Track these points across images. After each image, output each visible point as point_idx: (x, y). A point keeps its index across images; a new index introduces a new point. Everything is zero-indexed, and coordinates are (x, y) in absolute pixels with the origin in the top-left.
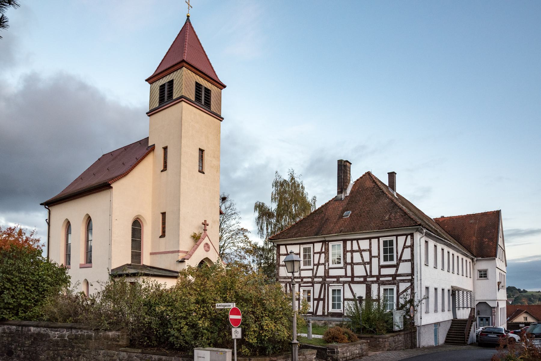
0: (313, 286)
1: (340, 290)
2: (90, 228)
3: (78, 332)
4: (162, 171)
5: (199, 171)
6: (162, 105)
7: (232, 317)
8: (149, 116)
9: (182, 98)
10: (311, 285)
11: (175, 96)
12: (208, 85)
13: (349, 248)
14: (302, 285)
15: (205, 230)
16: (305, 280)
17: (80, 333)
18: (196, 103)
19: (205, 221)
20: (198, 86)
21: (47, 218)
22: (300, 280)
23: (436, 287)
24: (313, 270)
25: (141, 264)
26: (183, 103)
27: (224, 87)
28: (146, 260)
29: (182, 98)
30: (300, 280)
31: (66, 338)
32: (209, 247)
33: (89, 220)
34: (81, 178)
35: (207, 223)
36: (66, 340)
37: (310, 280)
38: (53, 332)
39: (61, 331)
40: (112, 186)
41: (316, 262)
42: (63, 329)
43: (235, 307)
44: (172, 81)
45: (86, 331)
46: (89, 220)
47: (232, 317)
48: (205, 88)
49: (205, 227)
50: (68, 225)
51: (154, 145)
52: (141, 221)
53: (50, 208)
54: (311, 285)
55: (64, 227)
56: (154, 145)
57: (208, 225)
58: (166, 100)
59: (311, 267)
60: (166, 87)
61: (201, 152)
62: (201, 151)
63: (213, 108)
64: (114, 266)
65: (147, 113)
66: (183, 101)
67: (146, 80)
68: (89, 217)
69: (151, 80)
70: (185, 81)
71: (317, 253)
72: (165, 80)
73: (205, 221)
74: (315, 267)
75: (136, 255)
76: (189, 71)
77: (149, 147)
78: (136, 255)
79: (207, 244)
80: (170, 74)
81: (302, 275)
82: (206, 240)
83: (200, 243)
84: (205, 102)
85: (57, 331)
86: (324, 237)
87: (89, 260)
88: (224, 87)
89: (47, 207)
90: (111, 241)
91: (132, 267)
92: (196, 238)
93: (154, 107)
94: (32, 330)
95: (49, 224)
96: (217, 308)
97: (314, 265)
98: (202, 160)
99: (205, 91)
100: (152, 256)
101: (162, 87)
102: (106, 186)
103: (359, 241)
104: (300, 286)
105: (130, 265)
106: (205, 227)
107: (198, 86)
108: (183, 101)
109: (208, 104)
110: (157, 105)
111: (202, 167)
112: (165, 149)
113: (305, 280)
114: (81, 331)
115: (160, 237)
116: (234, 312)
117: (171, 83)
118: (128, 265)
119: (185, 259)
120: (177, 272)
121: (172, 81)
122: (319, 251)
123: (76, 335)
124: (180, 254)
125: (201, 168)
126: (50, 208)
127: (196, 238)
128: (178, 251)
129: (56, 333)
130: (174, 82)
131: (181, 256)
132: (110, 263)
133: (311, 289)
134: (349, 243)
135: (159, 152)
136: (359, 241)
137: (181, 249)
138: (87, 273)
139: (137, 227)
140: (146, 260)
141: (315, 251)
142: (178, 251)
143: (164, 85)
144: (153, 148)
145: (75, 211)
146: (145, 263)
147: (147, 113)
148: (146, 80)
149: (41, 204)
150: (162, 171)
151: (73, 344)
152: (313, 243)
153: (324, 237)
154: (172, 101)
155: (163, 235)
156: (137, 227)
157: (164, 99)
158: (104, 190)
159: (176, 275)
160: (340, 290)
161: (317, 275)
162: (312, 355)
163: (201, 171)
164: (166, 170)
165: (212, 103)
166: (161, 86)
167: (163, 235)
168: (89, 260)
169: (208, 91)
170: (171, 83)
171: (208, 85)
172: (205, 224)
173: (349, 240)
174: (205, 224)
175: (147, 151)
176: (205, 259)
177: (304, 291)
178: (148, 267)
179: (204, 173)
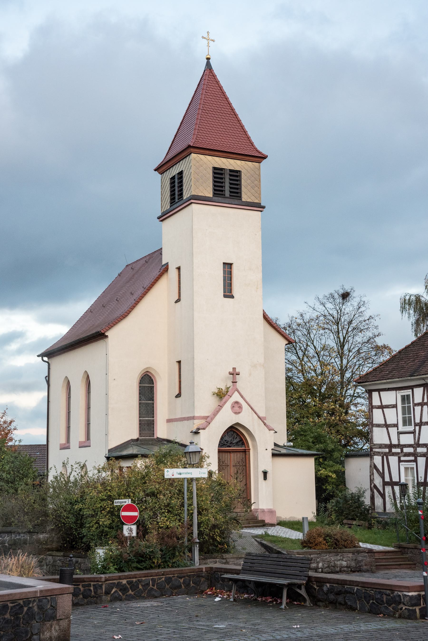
0: (415, 461)
1: (413, 468)
3: (16, 536)
7: (124, 514)
10: (412, 458)
13: (376, 402)
14: (403, 458)
15: (234, 382)
16: (406, 450)
17: (18, 537)
18: (216, 198)
19: (234, 369)
22: (398, 450)
24: (414, 432)
25: (155, 437)
30: (398, 450)
31: (6, 544)
32: (240, 407)
35: (237, 371)
36: (6, 546)
37: (411, 450)
39: (3, 536)
40: (106, 334)
41: (418, 421)
43: (130, 503)
44: (181, 173)
45: (22, 535)
47: (124, 514)
49: (234, 378)
52: (153, 376)
54: (412, 458)
58: (177, 200)
59: (411, 428)
64: (113, 444)
66: (192, 203)
71: (418, 404)
72: (174, 171)
73: (234, 369)
74: (417, 428)
79: (237, 403)
81: (402, 443)
82: (236, 397)
83: (225, 403)
86: (423, 379)
88: (264, 157)
89: (46, 359)
90: (107, 409)
92: (221, 395)
96: (115, 504)
97: (416, 425)
102: (99, 336)
103: (381, 392)
104: (400, 461)
106: (234, 378)
110: (167, 206)
112: (179, 268)
113: (406, 450)
114: (19, 535)
116: (128, 508)
117: (181, 173)
118: (132, 440)
119: (199, 429)
122: (420, 401)
123: (14, 540)
124: (196, 421)
127: (221, 395)
128: (193, 418)
131: (197, 423)
132: (107, 441)
133: (413, 465)
134: (375, 395)
136: (381, 392)
137: (196, 415)
139: (147, 385)
141: (416, 402)
142: (193, 418)
144: (165, 269)
146: (159, 436)
147: (159, 218)
148: (155, 170)
152: (412, 388)
153: (423, 379)
155: (179, 396)
156: (147, 385)
160: (413, 468)
161: (421, 442)
172: (234, 374)
173: (375, 390)
177: (406, 469)
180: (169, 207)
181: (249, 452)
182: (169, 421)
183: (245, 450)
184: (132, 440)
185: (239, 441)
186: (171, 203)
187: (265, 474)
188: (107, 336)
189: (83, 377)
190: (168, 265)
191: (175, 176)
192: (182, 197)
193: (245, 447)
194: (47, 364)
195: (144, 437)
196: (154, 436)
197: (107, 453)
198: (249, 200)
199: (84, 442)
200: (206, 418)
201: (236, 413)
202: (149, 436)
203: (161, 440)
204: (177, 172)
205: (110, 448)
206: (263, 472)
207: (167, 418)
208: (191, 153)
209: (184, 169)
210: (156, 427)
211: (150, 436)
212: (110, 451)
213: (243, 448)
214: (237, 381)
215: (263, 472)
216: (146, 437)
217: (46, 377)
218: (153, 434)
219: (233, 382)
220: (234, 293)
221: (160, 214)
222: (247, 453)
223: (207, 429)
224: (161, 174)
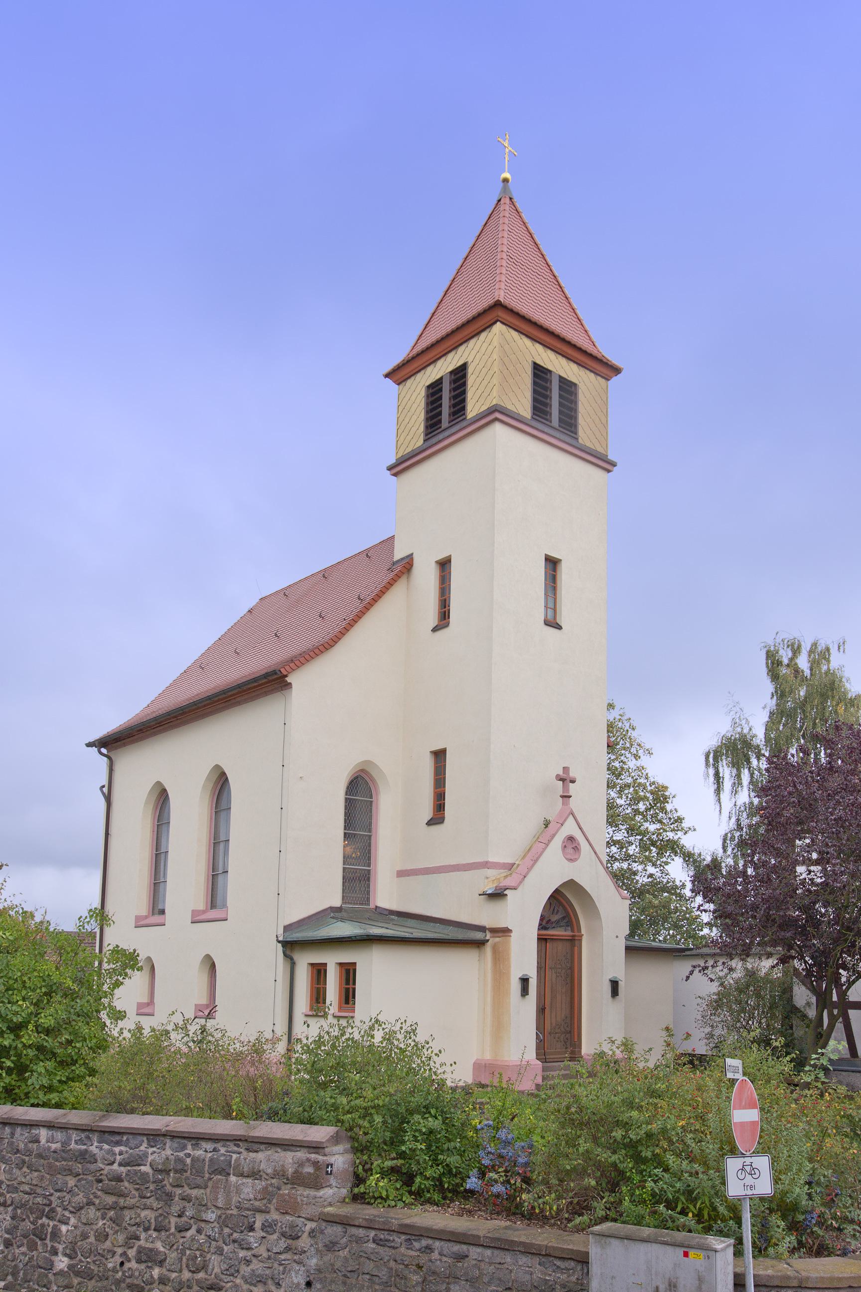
2: (223, 806)
3: (184, 1148)
4: (435, 630)
5: (547, 623)
6: (434, 440)
8: (395, 475)
9: (496, 414)
11: (473, 408)
12: (560, 366)
15: (566, 797)
18: (534, 423)
19: (566, 769)
20: (540, 373)
21: (105, 782)
23: (555, 555)
25: (372, 906)
26: (498, 426)
27: (617, 371)
28: (386, 893)
29: (496, 414)
32: (577, 849)
33: (220, 784)
34: (200, 665)
35: (572, 774)
38: (106, 1147)
40: (288, 680)
42: (140, 1138)
44: (463, 368)
46: (220, 784)
48: (562, 379)
49: (566, 789)
50: (161, 797)
51: (411, 556)
53: (111, 755)
55: (151, 807)
56: (411, 556)
57: (573, 781)
58: (445, 424)
60: (538, 380)
61: (550, 566)
62: (552, 563)
63: (585, 435)
65: (390, 469)
66: (496, 419)
67: (387, 376)
68: (223, 774)
69: (399, 374)
70: (497, 365)
73: (566, 769)
75: (357, 878)
76: (515, 334)
77: (394, 564)
78: (357, 878)
79: (571, 839)
80: (456, 348)
82: (570, 828)
84: (560, 420)
85: (118, 1143)
87: (215, 897)
88: (617, 371)
89: (104, 751)
91: (344, 914)
93: (409, 450)
94: (43, 1141)
95: (108, 799)
98: (554, 589)
99: (560, 388)
100: (404, 879)
101: (434, 390)
102: (272, 683)
105: (339, 910)
106: (566, 789)
107: (540, 373)
108: (496, 419)
109: (571, 425)
110: (419, 441)
111: (555, 610)
112: (444, 565)
115: (429, 823)
117: (460, 375)
118: (332, 909)
120: (482, 929)
121: (463, 368)
125: (550, 612)
126: (111, 755)
128: (486, 865)
129: (117, 1150)
130: (470, 370)
135: (425, 575)
137: (491, 859)
138: (210, 938)
139: (360, 791)
140: (386, 893)
143: (439, 381)
144: (407, 566)
145: (176, 765)
147: (390, 469)
148: (387, 376)
149: (89, 745)
150: (435, 630)
151: (168, 1188)
154: (464, 424)
155: (438, 817)
156: (360, 791)
157: (440, 421)
158: (266, 694)
159: (479, 936)
162: (860, 1111)
163: (553, 623)
164: (447, 625)
165: (581, 420)
166: (429, 387)
167: (438, 817)
168: (215, 897)
169: (568, 388)
170: (460, 375)
171: (560, 366)
174: (565, 779)
175: (392, 575)
176: (565, 884)
178: (392, 912)
179: (559, 627)
180: (421, 442)
181: (580, 940)
182: (401, 874)
183: (573, 936)
184: (331, 908)
185: (564, 918)
186: (426, 435)
187: (615, 986)
188: (290, 684)
189: (208, 778)
190: (412, 559)
191: (441, 378)
192: (464, 414)
193: (573, 931)
194: (105, 759)
195: (351, 903)
196: (369, 904)
197: (281, 931)
198: (588, 444)
199: (204, 912)
200: (510, 867)
201: (571, 860)
202: (360, 904)
203: (387, 913)
204: (450, 369)
205: (287, 923)
206: (611, 981)
207: (399, 868)
208: (495, 323)
209: (470, 360)
210: (375, 885)
211: (362, 904)
212: (287, 928)
213: (569, 933)
214: (570, 794)
215: (611, 981)
216: (354, 904)
217: (103, 786)
218: (368, 899)
219: (562, 797)
220: (563, 621)
221: (393, 461)
222: (577, 943)
223: (520, 889)
224: (398, 384)
